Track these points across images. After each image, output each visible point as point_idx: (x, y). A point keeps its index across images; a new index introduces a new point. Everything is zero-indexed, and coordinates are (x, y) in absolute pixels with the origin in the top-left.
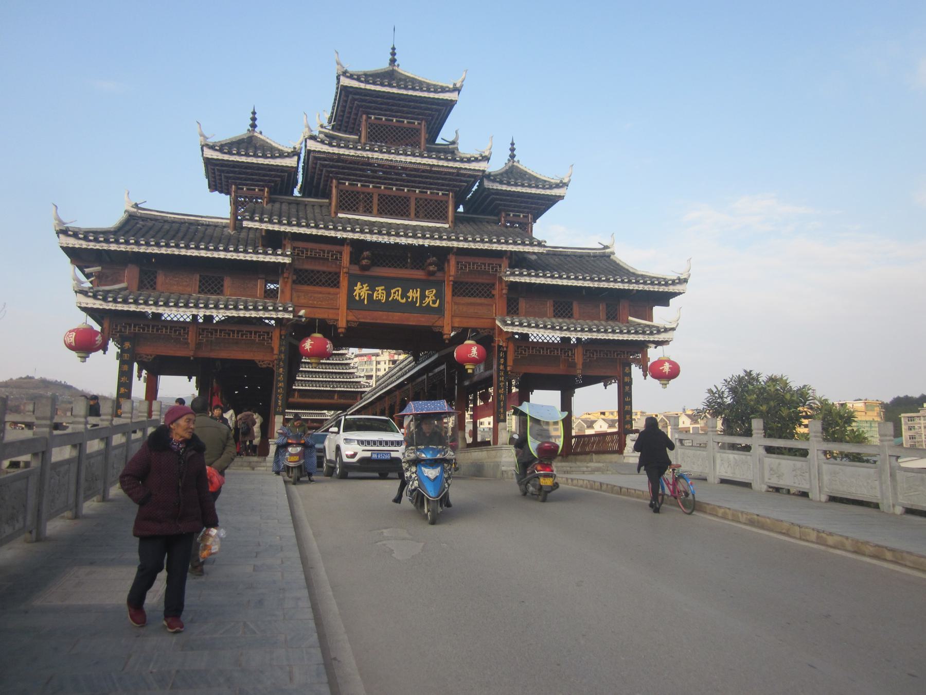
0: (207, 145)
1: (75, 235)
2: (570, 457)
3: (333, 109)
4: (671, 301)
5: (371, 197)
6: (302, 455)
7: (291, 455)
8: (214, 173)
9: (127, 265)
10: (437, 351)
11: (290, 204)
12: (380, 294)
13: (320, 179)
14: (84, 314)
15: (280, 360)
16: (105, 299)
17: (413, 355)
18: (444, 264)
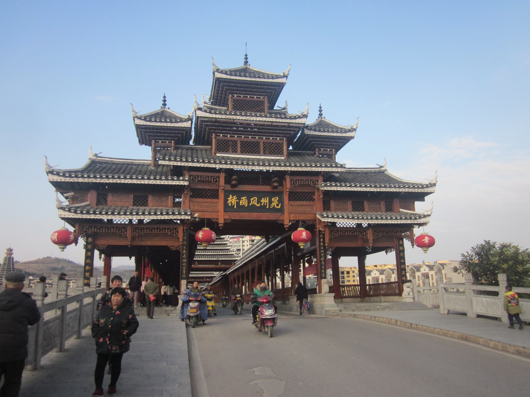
1: (58, 174)
2: (367, 298)
4: (425, 197)
5: (236, 143)
6: (199, 308)
7: (192, 308)
8: (141, 134)
10: (280, 235)
12: (244, 201)
14: (63, 221)
15: (183, 245)
16: (75, 212)
18: (282, 181)
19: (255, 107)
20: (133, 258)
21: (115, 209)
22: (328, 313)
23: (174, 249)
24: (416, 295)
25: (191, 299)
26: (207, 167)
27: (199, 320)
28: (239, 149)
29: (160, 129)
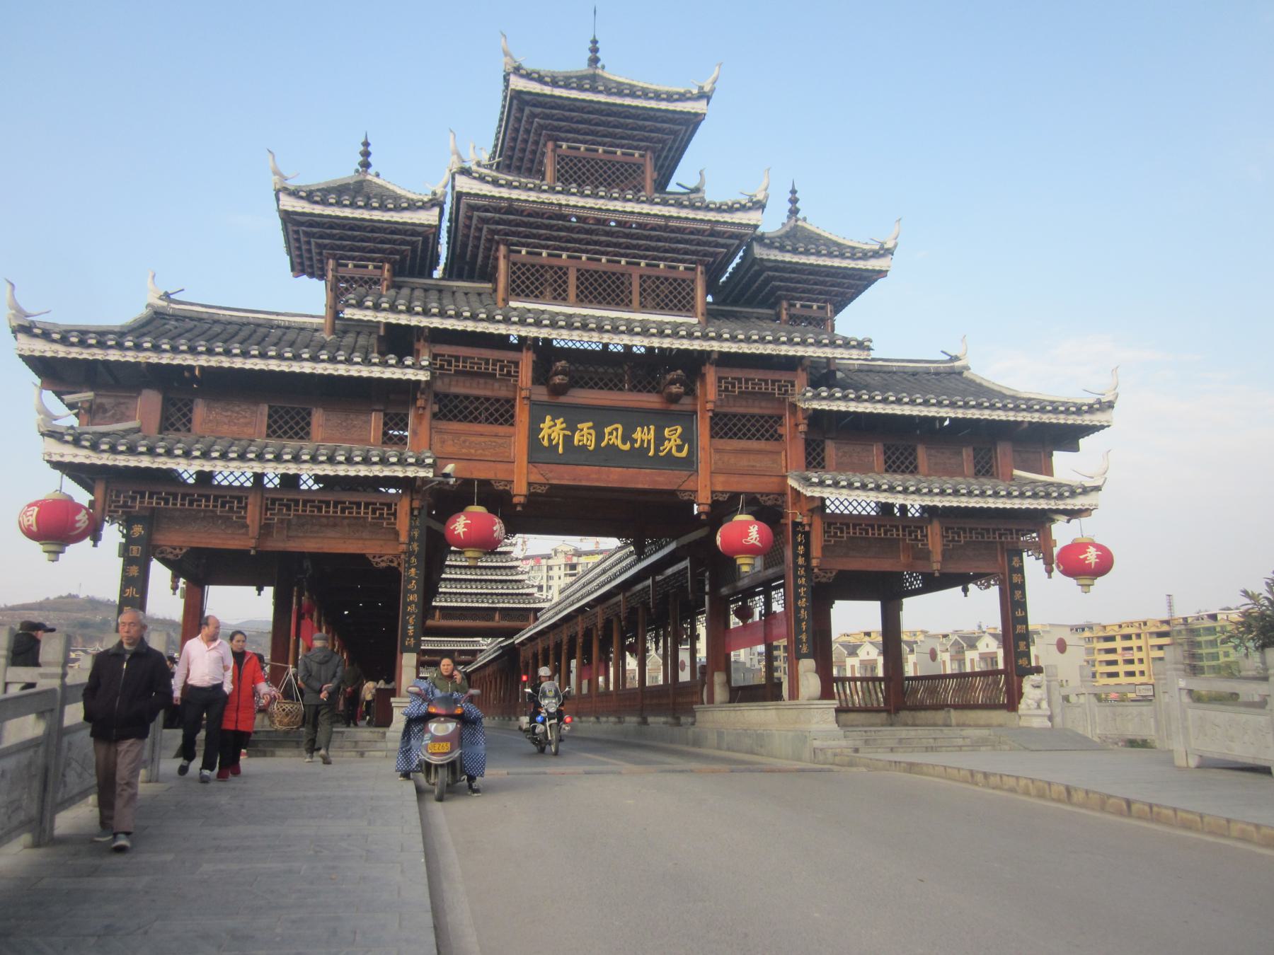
0: (285, 190)
1: (46, 335)
2: (904, 715)
3: (497, 139)
4: (1081, 441)
5: (565, 274)
6: (458, 739)
7: (436, 739)
8: (298, 240)
9: (136, 387)
10: (674, 538)
11: (426, 290)
12: (585, 435)
13: (477, 247)
14: (58, 473)
15: (410, 554)
16: (94, 447)
17: (633, 544)
18: (694, 383)
19: (619, 177)
20: (269, 591)
21: (214, 443)
22: (821, 758)
23: (383, 565)
24: (1057, 711)
25: (433, 710)
26: (483, 334)
27: (458, 778)
28: (572, 291)
29: (352, 229)
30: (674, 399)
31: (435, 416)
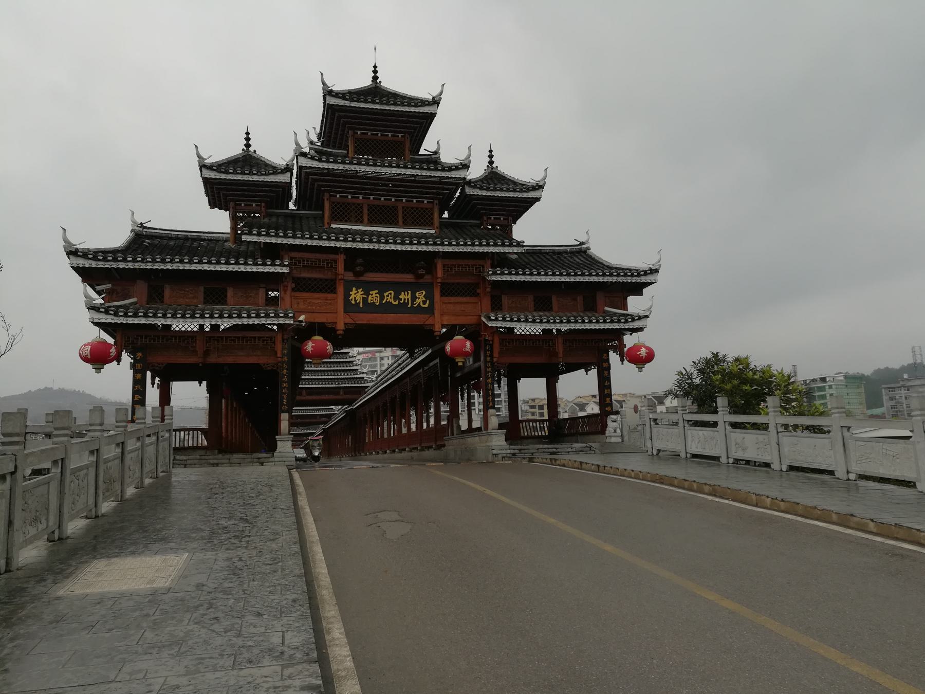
14: (97, 329)
16: (116, 314)
30: (422, 276)
31: (293, 290)
